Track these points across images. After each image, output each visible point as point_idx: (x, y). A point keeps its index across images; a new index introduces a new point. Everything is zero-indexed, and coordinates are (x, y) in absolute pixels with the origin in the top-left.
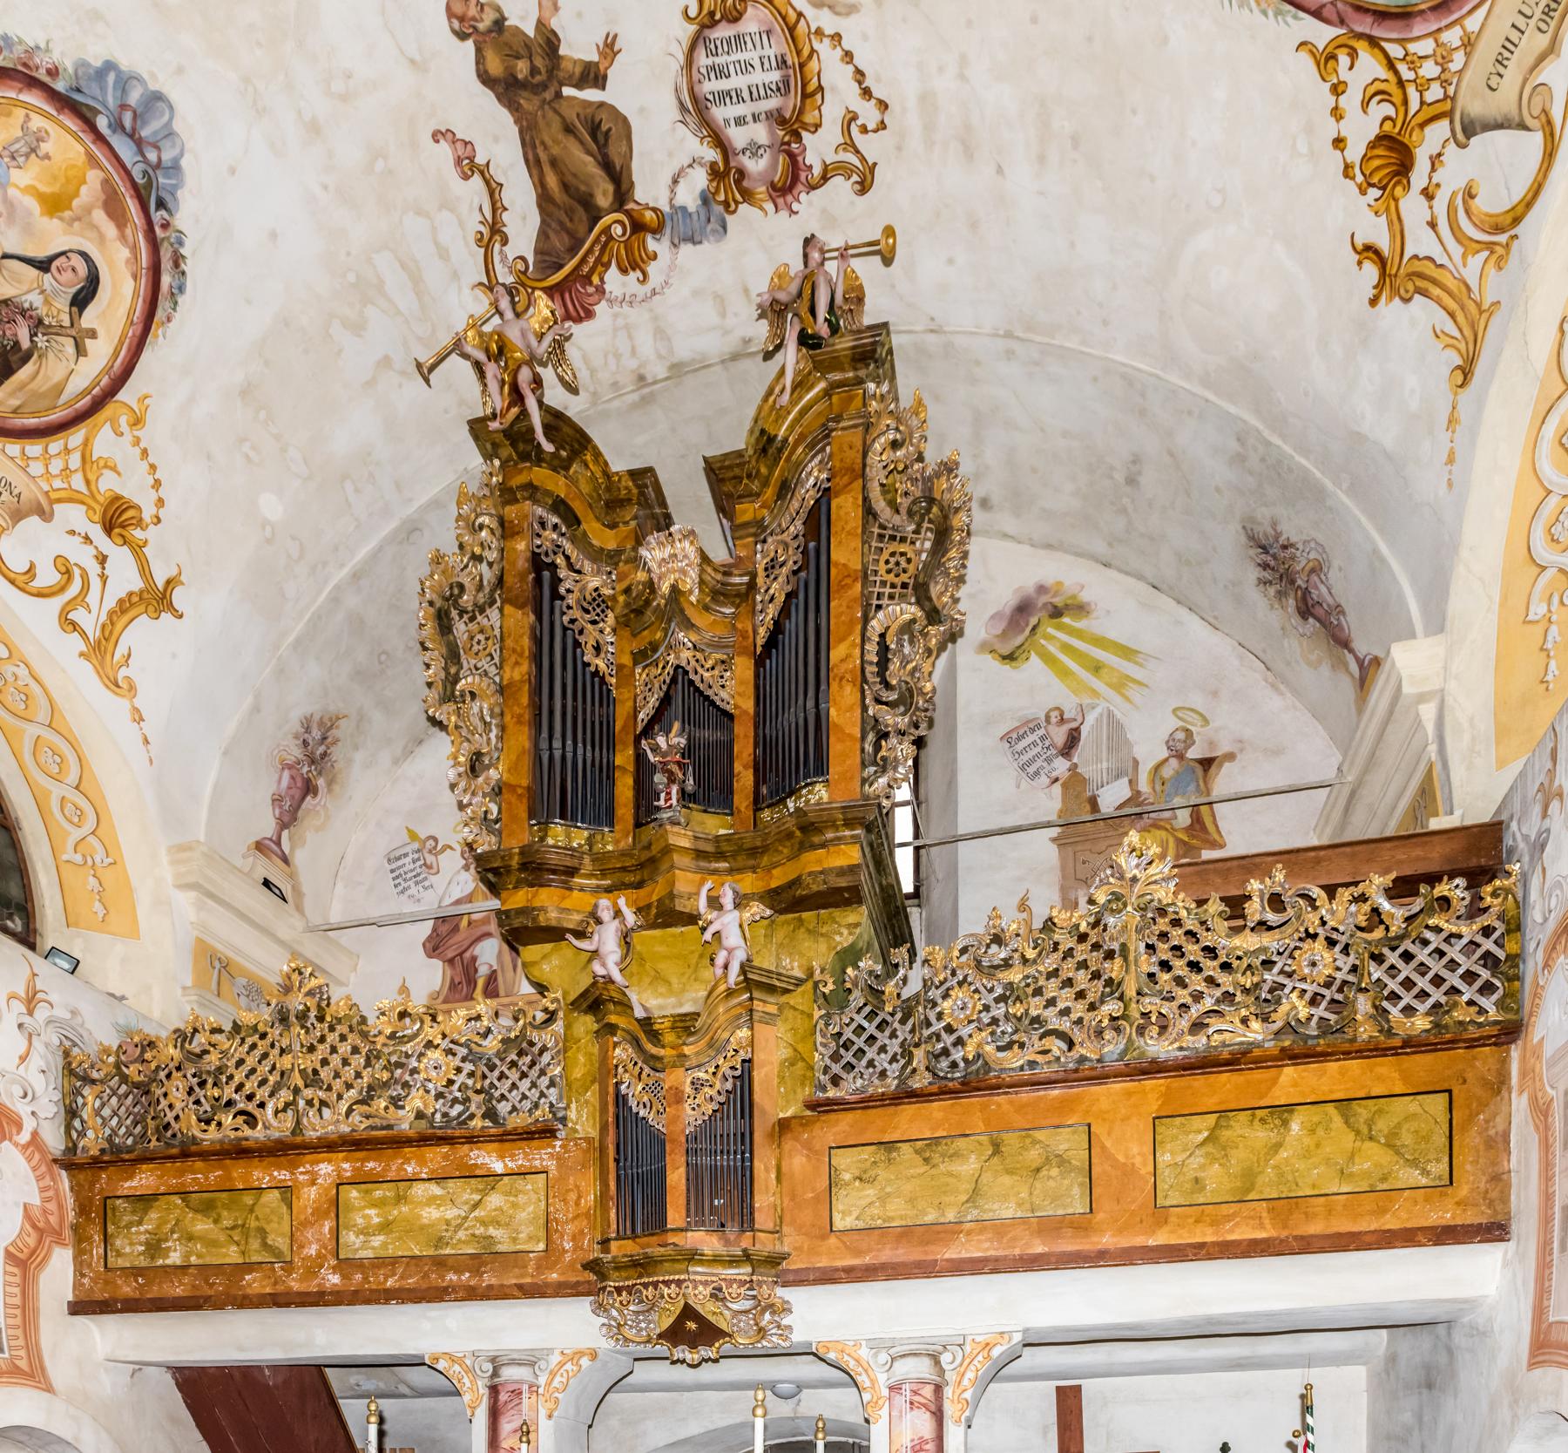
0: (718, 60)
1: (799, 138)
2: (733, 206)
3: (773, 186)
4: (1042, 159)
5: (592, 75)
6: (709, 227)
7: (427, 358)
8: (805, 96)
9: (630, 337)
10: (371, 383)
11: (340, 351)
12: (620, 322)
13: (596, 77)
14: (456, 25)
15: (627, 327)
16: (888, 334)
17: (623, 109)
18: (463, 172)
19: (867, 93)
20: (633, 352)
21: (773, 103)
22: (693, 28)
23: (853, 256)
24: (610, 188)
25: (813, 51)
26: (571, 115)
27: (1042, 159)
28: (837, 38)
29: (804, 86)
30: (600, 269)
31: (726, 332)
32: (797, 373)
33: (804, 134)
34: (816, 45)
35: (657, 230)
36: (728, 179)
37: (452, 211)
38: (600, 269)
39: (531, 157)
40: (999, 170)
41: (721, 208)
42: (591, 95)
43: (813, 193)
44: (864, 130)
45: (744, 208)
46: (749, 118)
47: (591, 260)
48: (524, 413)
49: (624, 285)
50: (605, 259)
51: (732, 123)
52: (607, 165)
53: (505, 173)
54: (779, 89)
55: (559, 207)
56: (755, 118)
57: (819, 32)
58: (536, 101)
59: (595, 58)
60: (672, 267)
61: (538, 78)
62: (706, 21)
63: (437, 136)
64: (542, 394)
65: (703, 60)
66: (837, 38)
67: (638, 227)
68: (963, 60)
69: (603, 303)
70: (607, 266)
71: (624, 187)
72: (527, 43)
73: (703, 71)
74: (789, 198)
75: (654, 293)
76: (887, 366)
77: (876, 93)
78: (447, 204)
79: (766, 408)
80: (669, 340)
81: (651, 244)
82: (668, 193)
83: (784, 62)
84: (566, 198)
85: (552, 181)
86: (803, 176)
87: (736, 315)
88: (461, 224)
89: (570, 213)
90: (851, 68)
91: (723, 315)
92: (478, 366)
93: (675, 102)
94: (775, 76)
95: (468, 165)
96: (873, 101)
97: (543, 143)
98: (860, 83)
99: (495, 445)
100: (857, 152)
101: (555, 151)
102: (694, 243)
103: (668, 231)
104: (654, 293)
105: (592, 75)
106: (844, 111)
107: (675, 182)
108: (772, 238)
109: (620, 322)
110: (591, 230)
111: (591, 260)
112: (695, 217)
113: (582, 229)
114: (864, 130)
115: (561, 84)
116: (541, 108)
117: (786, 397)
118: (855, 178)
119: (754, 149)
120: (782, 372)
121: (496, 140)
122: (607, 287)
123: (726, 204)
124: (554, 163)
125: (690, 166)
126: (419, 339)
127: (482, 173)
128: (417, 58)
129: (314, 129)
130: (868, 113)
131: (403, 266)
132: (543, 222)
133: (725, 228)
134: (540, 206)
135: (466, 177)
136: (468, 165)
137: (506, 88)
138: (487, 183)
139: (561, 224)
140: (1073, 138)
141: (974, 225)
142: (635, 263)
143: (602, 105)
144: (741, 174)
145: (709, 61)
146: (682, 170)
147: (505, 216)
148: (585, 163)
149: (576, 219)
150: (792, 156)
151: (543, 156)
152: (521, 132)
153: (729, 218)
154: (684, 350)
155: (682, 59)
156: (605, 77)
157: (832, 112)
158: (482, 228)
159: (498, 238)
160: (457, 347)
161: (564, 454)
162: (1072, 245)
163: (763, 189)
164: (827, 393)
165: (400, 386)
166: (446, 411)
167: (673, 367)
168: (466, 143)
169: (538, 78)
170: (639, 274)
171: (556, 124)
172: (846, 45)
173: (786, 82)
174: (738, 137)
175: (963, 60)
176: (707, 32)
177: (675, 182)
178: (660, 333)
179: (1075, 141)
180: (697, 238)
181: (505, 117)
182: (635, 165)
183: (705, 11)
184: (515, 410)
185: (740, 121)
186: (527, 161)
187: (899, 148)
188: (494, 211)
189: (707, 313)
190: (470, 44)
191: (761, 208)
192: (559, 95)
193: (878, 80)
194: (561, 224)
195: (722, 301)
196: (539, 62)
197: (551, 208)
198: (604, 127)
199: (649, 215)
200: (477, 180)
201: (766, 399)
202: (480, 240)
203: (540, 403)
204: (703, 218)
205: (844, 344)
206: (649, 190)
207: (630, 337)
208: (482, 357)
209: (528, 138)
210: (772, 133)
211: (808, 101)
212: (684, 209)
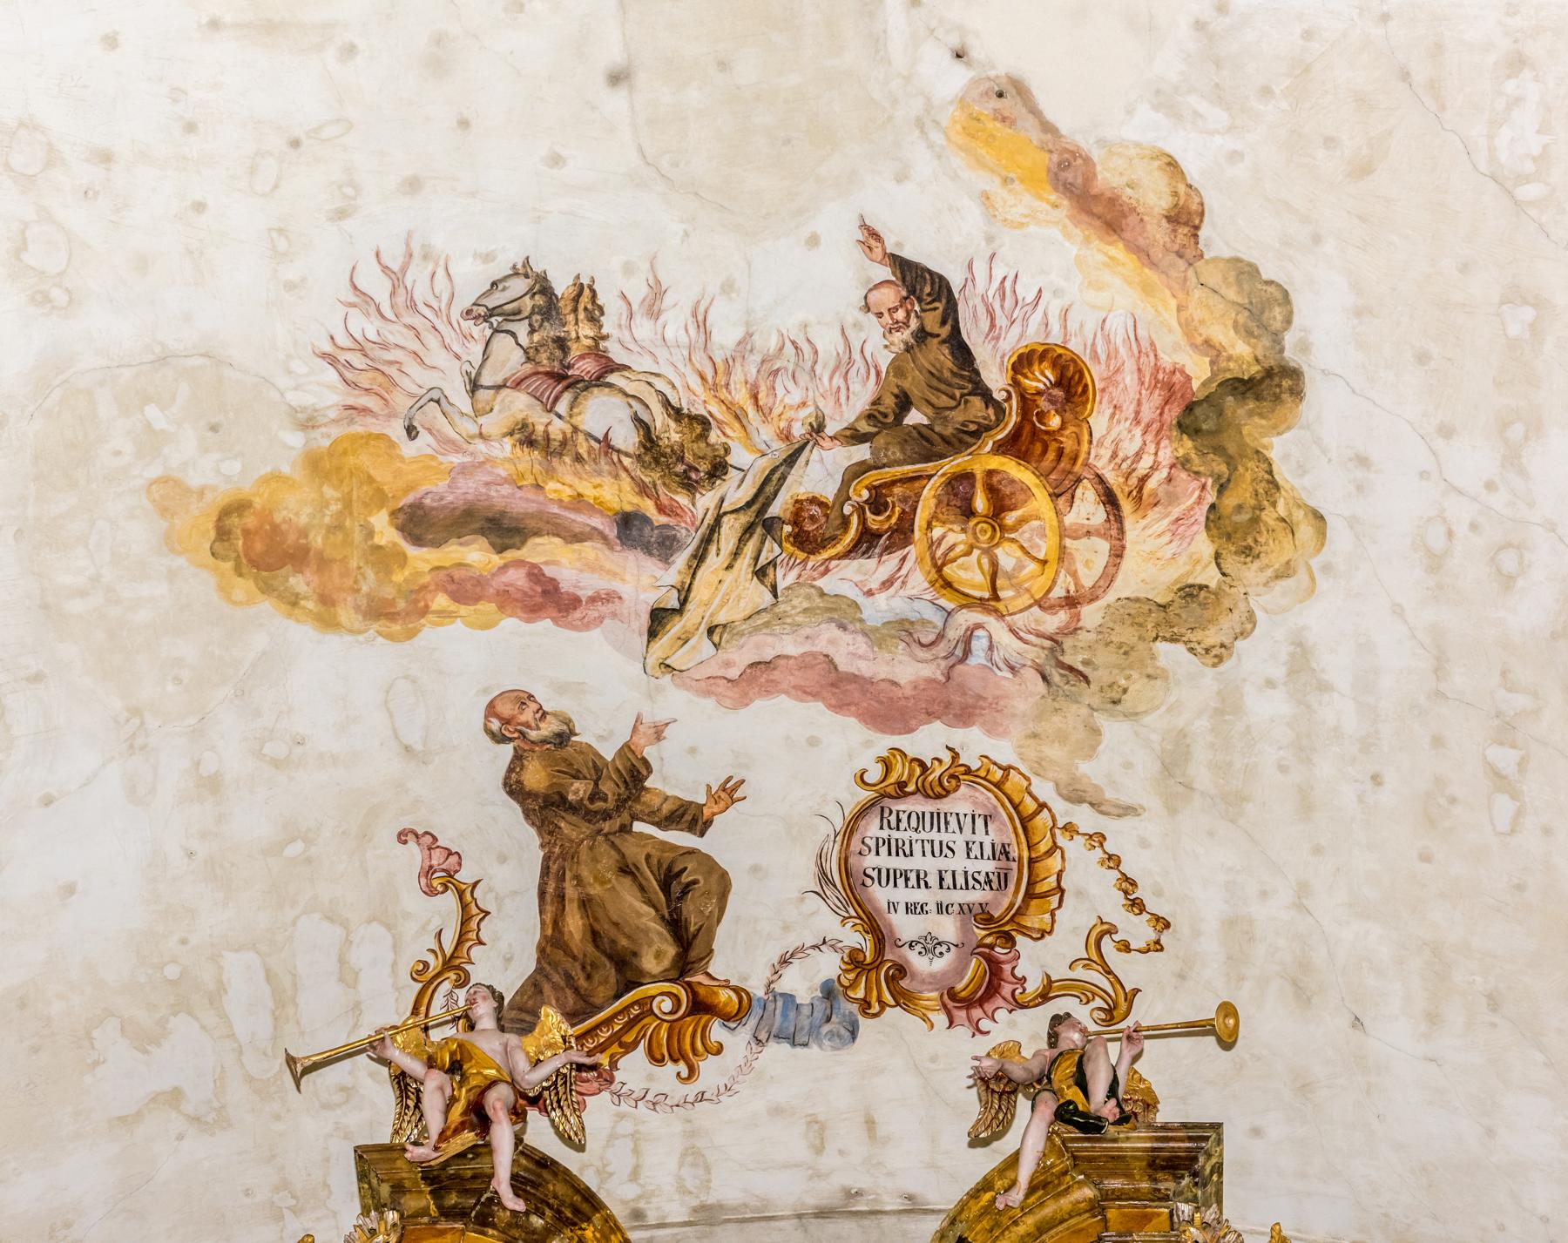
0: (895, 834)
1: (1009, 940)
2: (876, 1008)
3: (952, 995)
4: (1433, 1018)
5: (688, 817)
6: (826, 1028)
7: (306, 1051)
8: (1030, 895)
9: (636, 1151)
10: (126, 1121)
11: (96, 1063)
12: (626, 1127)
13: (694, 820)
14: (495, 725)
15: (635, 1137)
16: (1219, 1141)
17: (723, 861)
18: (430, 886)
19: (1137, 906)
20: (635, 1175)
21: (976, 896)
22: (866, 795)
23: (1147, 1037)
24: (671, 951)
25: (1055, 846)
26: (635, 853)
27: (1433, 1018)
28: (1098, 839)
29: (1031, 884)
30: (615, 1048)
31: (817, 1175)
32: (1042, 1169)
33: (1019, 938)
34: (1062, 840)
35: (733, 1018)
36: (877, 975)
37: (389, 927)
38: (615, 1048)
39: (551, 889)
40: (1357, 1022)
41: (855, 1008)
42: (679, 838)
43: (1020, 1012)
44: (1125, 947)
45: (894, 1014)
46: (932, 907)
47: (604, 1035)
48: (483, 1149)
49: (650, 1078)
50: (629, 1038)
51: (901, 908)
52: (676, 925)
53: (499, 900)
54: (989, 882)
55: (575, 958)
56: (940, 908)
57: (1069, 828)
58: (587, 829)
59: (701, 799)
60: (746, 1067)
61: (599, 805)
62: (890, 790)
63: (402, 837)
64: (523, 1130)
65: (872, 829)
66: (1098, 839)
67: (701, 1006)
68: (1303, 889)
69: (606, 1095)
70: (630, 1048)
71: (693, 954)
72: (598, 769)
73: (872, 843)
74: (977, 1013)
75: (701, 1097)
76: (1210, 1189)
77: (1151, 906)
78: (385, 916)
79: (975, 1208)
80: (708, 1169)
81: (717, 1031)
82: (768, 973)
83: (1007, 854)
84: (590, 948)
85: (574, 924)
86: (1006, 989)
87: (841, 1152)
88: (396, 947)
89: (589, 969)
90: (1115, 874)
91: (819, 1150)
92: (402, 1081)
93: (814, 869)
94: (989, 866)
95: (442, 875)
96: (1145, 916)
97: (577, 877)
98: (1126, 893)
99: (398, 1189)
100: (1108, 971)
101: (595, 890)
102: (794, 1044)
103: (752, 1022)
104: (701, 1097)
105: (688, 817)
106: (1094, 921)
107: (784, 962)
108: (933, 1059)
109: (626, 1127)
110: (618, 996)
111: (604, 1035)
112: (806, 1011)
113: (602, 993)
114: (1125, 947)
115: (634, 817)
116: (593, 837)
117: (1017, 1196)
118: (1099, 1002)
119: (930, 945)
120: (1014, 1160)
121: (503, 859)
122: (619, 1076)
123: (865, 1004)
124: (585, 904)
125: (816, 947)
126: (250, 1079)
127: (461, 894)
128: (419, 747)
129: (212, 785)
130: (1138, 930)
131: (269, 976)
132: (539, 970)
133: (853, 1034)
134: (541, 950)
135: (431, 892)
136: (442, 875)
137: (544, 809)
138: (464, 907)
139: (568, 977)
140: (1490, 997)
141: (1304, 1088)
142: (679, 1051)
143: (691, 852)
144: (901, 970)
145: (885, 834)
146: (802, 949)
147: (476, 952)
148: (638, 913)
149: (596, 978)
150: (994, 967)
151: (571, 891)
152: (546, 859)
153: (862, 1021)
154: (727, 1190)
155: (839, 824)
156: (708, 823)
157: (1073, 921)
158: (431, 959)
159: (452, 975)
160: (375, 1048)
161: (537, 1222)
162: (1490, 1132)
163: (935, 995)
164: (1096, 1208)
165: (180, 1137)
166: (247, 1193)
167: (703, 1208)
168: (450, 854)
169: (599, 805)
170: (683, 1068)
171: (608, 860)
172: (1110, 847)
173: (1003, 879)
174: (905, 927)
175: (1303, 889)
176: (887, 802)
177: (784, 962)
178: (693, 1155)
179: (1494, 1002)
180: (800, 1038)
181: (530, 838)
182: (722, 931)
183: (892, 779)
184: (468, 1138)
185: (911, 908)
186: (542, 894)
187: (1182, 977)
188: (460, 942)
189: (793, 1143)
190: (507, 750)
191: (925, 1019)
192: (625, 829)
193: (1159, 893)
194: (568, 977)
195: (823, 1128)
196: (607, 788)
197: (559, 955)
198: (685, 878)
199: (724, 996)
200: (449, 900)
201: (975, 1194)
202: (419, 973)
203: (518, 1140)
204: (818, 1014)
205: (1135, 1141)
206: (736, 959)
207: (636, 1151)
208: (415, 1067)
209: (554, 868)
210: (965, 929)
211: (1034, 903)
212: (789, 998)
